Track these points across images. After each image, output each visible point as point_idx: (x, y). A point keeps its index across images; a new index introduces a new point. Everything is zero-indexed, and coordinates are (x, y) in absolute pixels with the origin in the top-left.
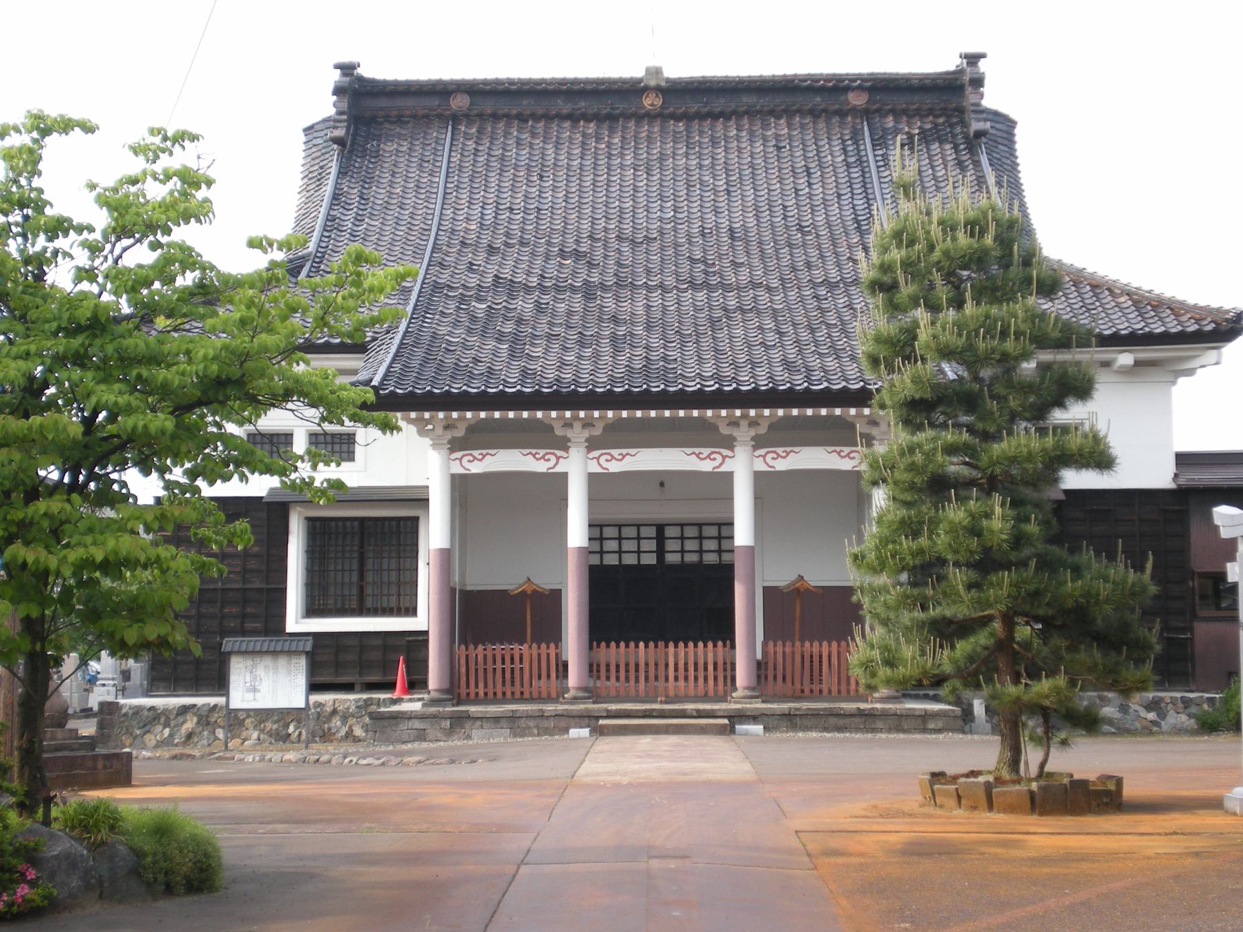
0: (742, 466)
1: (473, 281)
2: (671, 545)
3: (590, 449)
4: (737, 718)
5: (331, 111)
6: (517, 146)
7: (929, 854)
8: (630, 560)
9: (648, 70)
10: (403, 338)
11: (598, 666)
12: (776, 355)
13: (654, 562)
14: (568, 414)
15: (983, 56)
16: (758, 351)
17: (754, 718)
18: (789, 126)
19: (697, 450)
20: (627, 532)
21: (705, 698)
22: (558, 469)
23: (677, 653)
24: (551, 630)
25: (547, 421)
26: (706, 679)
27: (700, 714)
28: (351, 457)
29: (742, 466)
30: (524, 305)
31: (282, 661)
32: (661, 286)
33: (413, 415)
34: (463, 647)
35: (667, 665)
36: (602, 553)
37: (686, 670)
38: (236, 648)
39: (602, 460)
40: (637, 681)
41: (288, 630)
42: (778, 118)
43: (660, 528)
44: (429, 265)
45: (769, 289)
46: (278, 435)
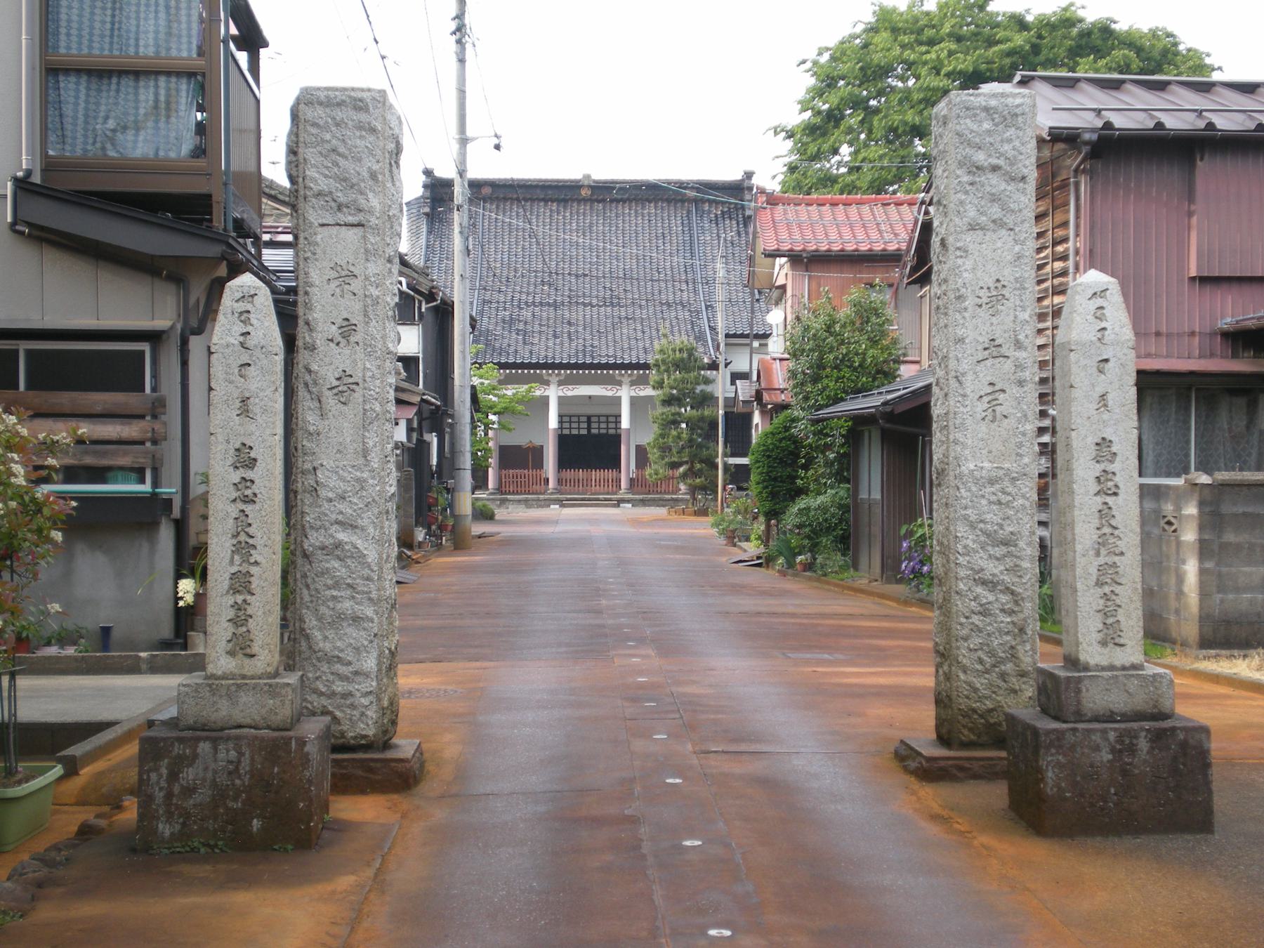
0: (625, 394)
4: (620, 502)
7: (47, 40)
8: (575, 432)
12: (641, 345)
16: (633, 342)
17: (628, 501)
18: (656, 208)
20: (574, 419)
21: (608, 493)
23: (596, 474)
24: (539, 463)
26: (80, 36)
27: (606, 500)
29: (625, 394)
30: (527, 314)
42: (650, 202)
43: (589, 418)
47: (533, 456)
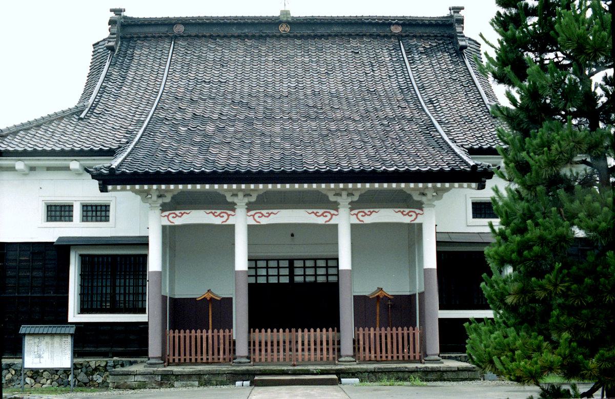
0: (344, 220)
1: (179, 116)
2: (298, 272)
3: (248, 210)
5: (107, 34)
6: (210, 52)
8: (273, 280)
9: (282, 12)
10: (136, 145)
11: (254, 342)
13: (288, 281)
14: (234, 186)
15: (463, 8)
19: (315, 211)
22: (229, 222)
25: (222, 193)
26: (322, 350)
28: (106, 219)
30: (210, 128)
31: (57, 340)
32: (290, 118)
33: (137, 187)
34: (172, 331)
35: (297, 342)
36: (256, 276)
37: (309, 345)
38: (27, 332)
39: (256, 217)
40: (278, 351)
41: (70, 321)
43: (291, 261)
44: (156, 109)
45: (354, 120)
46: (65, 206)
47: (216, 312)
